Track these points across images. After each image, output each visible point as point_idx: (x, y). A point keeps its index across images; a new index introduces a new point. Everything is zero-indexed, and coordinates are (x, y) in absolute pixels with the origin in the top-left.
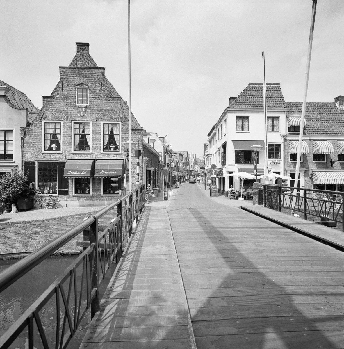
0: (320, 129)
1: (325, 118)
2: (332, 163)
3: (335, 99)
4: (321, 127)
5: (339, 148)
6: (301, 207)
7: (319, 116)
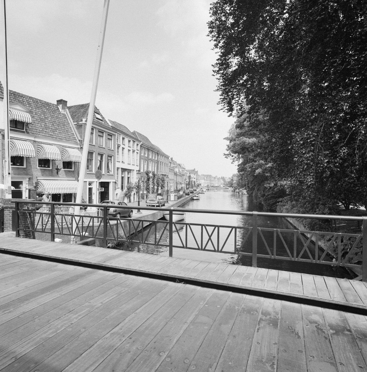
0: (45, 131)
1: (49, 119)
2: (58, 170)
3: (58, 101)
4: (46, 128)
5: (65, 155)
6: (38, 225)
7: (42, 115)
